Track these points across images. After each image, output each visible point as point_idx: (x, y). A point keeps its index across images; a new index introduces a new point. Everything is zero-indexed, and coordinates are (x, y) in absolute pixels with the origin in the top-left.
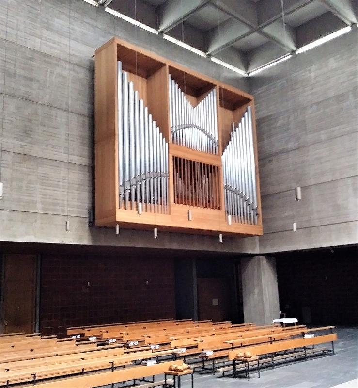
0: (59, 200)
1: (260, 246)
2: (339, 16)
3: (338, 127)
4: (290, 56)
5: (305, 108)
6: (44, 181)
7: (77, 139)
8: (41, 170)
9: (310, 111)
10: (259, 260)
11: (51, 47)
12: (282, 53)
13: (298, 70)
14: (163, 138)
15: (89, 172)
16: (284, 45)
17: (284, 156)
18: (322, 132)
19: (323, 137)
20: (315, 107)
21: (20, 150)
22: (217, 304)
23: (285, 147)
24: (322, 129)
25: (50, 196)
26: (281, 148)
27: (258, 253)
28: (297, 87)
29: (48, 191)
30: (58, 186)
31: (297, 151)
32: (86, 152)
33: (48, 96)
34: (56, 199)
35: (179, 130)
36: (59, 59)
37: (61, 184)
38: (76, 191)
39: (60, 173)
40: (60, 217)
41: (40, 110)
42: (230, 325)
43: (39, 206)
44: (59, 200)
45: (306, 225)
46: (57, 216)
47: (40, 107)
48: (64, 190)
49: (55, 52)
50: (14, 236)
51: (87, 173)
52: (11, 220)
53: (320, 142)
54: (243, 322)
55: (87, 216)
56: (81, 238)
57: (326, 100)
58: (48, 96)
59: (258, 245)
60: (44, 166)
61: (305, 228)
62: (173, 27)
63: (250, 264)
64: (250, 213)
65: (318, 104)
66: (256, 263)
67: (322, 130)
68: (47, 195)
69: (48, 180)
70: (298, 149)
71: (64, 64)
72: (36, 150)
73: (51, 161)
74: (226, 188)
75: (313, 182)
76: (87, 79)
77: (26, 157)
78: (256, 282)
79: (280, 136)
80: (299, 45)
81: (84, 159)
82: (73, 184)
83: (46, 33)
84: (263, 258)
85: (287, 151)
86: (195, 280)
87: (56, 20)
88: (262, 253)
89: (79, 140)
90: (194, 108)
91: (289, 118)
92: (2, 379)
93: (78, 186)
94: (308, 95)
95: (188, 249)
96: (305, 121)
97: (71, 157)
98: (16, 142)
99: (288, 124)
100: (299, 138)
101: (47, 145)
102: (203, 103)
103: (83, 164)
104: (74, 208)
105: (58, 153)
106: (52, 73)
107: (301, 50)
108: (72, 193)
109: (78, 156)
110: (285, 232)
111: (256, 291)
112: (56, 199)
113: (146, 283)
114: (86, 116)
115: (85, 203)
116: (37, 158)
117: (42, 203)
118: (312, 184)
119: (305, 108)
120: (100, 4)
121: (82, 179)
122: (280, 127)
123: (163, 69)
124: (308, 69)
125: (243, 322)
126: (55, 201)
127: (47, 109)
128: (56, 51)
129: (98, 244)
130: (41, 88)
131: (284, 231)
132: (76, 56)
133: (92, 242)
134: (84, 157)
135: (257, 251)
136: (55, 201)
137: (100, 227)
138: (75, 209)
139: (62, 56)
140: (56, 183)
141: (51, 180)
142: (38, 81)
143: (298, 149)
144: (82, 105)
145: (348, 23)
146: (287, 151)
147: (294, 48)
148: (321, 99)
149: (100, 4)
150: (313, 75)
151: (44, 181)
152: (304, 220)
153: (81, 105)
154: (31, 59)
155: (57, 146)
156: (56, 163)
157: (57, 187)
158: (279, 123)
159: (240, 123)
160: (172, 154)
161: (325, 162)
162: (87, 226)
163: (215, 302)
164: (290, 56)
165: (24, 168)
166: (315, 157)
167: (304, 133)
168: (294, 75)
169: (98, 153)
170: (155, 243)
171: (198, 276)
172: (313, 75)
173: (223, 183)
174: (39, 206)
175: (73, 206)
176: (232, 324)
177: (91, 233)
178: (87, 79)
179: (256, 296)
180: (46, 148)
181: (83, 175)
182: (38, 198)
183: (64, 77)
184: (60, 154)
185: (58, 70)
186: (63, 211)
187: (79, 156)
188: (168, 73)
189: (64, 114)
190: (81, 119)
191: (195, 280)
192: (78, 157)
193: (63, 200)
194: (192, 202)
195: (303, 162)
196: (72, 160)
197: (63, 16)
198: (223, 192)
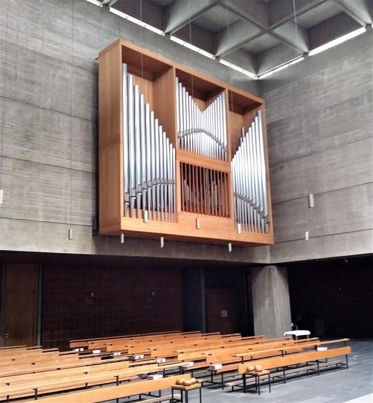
0: (61, 208)
1: (271, 255)
2: (353, 17)
3: (352, 132)
4: (302, 58)
5: (318, 112)
6: (46, 188)
7: (80, 144)
8: (42, 177)
9: (323, 116)
10: (270, 270)
11: (53, 49)
12: (293, 55)
13: (311, 73)
14: (170, 144)
15: (93, 179)
16: (295, 47)
17: (296, 162)
18: (336, 137)
19: (337, 142)
20: (328, 111)
21: (21, 156)
22: (226, 316)
23: (297, 153)
24: (335, 134)
25: (52, 203)
26: (293, 154)
27: (269, 263)
28: (310, 90)
29: (50, 199)
30: (60, 193)
31: (309, 157)
32: (90, 158)
33: (50, 100)
34: (58, 207)
35: (186, 135)
36: (61, 62)
37: (63, 191)
38: (79, 199)
39: (62, 180)
40: (63, 226)
41: (42, 114)
42: (240, 338)
43: (41, 213)
44: (61, 208)
45: (319, 234)
46: (59, 224)
47: (41, 111)
48: (66, 197)
49: (58, 54)
50: (15, 245)
51: (90, 180)
52: (11, 229)
53: (333, 147)
54: (253, 335)
55: (91, 224)
56: (84, 248)
57: (339, 104)
58: (50, 100)
59: (269, 255)
60: (46, 172)
61: (318, 237)
62: (180, 28)
63: (260, 274)
64: (261, 222)
65: (331, 108)
66: (267, 273)
67: (336, 135)
68: (49, 203)
69: (50, 187)
70: (310, 154)
71: (66, 66)
72: (38, 156)
73: (53, 167)
74: (236, 195)
75: (326, 189)
76: (90, 82)
77: (27, 163)
78: (266, 293)
79: (291, 141)
80: (311, 47)
81: (88, 165)
82: (76, 191)
83: (48, 35)
84: (275, 268)
85: (299, 157)
86: (203, 291)
87: (59, 20)
88: (273, 263)
89: (82, 146)
90: (202, 112)
91: (301, 122)
92: (2, 393)
93: (81, 193)
94: (321, 99)
95: (196, 259)
96: (317, 126)
97: (74, 163)
98: (16, 147)
99: (300, 129)
100: (311, 144)
101: (49, 150)
102: (211, 107)
103: (87, 170)
104: (77, 216)
105: (61, 159)
106: (54, 75)
107: (313, 52)
108: (76, 200)
109: (81, 162)
110: (297, 241)
111: (267, 302)
112: (58, 207)
113: (152, 294)
114: (89, 121)
115: (89, 211)
116: (39, 164)
117: (44, 210)
118: (325, 191)
119: (318, 112)
120: (104, 4)
121: (85, 185)
122: (291, 132)
123: (170, 71)
124: (321, 71)
125: (253, 335)
126: (58, 209)
127: (49, 113)
128: (58, 53)
129: (102, 253)
130: (43, 92)
131: (295, 240)
132: (79, 59)
133: (96, 252)
134: (87, 163)
135: (268, 261)
136: (58, 209)
137: (104, 236)
138: (78, 217)
139: (65, 58)
140: (59, 190)
141: (53, 187)
142: (40, 84)
143: (310, 154)
144: (86, 109)
145: (362, 24)
146: (299, 157)
147: (306, 50)
148: (335, 103)
149: (104, 4)
150: (326, 77)
151: (46, 188)
152: (317, 228)
153: (84, 109)
154: (33, 61)
155: (59, 151)
156: (58, 169)
157: (60, 195)
158: (291, 128)
159: (250, 128)
160: (179, 160)
161: (339, 168)
162: (91, 234)
163: (224, 314)
164: (302, 58)
165: (25, 174)
166: (328, 163)
167: (317, 138)
168: (307, 78)
169: (102, 158)
170: (161, 252)
171: (206, 287)
172: (326, 77)
173: (232, 190)
174: (41, 213)
175: (76, 214)
176: (242, 337)
177: (95, 242)
178: (90, 82)
179: (267, 307)
180: (47, 153)
181: (86, 182)
182: (40, 205)
183: (67, 80)
184: (62, 160)
185: (60, 73)
186: (66, 219)
187: (82, 162)
188: (175, 76)
189: (67, 118)
190: (85, 123)
191: (203, 291)
192: (82, 163)
193: (66, 208)
194: (200, 210)
195: (316, 168)
196: (75, 166)
197: (65, 17)
198: (233, 199)
